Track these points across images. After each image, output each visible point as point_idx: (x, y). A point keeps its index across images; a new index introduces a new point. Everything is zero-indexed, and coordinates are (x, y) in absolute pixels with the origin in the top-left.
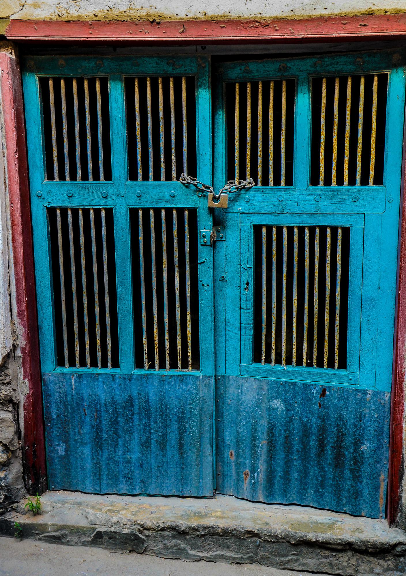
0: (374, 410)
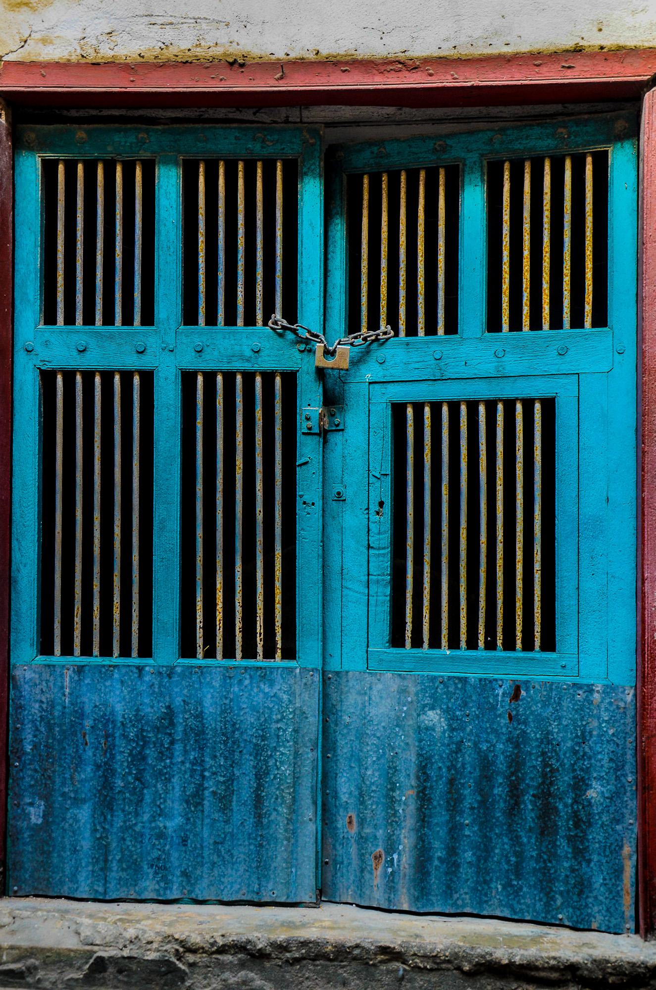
0: (606, 721)
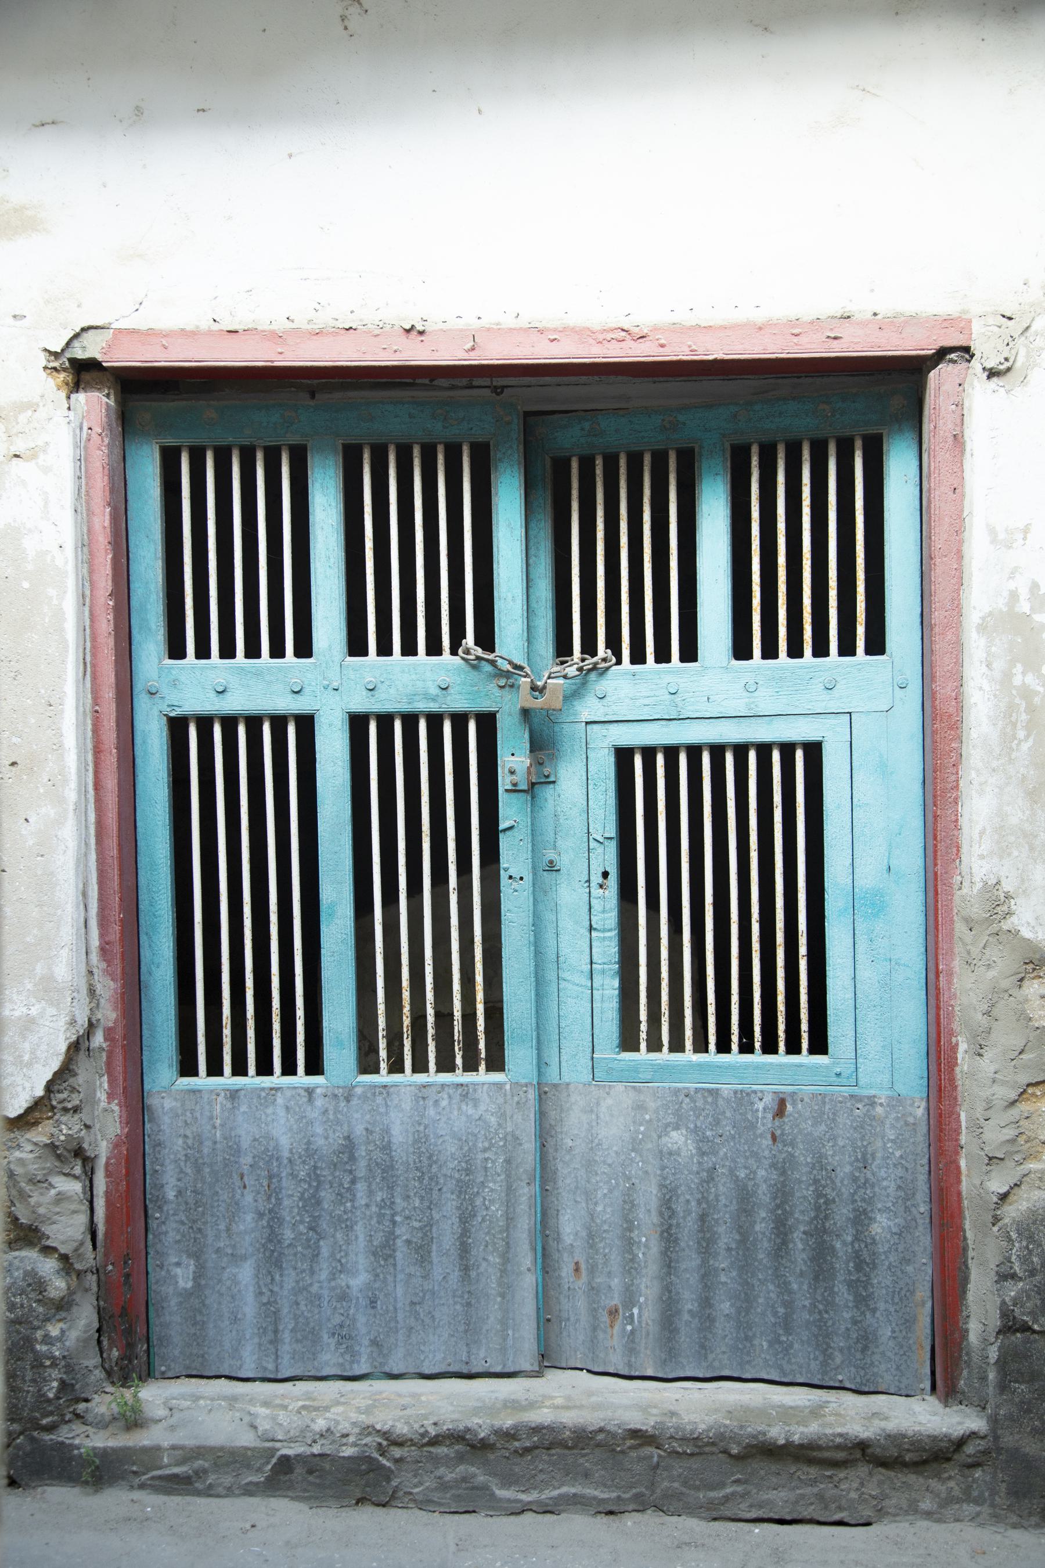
0: (892, 1141)
